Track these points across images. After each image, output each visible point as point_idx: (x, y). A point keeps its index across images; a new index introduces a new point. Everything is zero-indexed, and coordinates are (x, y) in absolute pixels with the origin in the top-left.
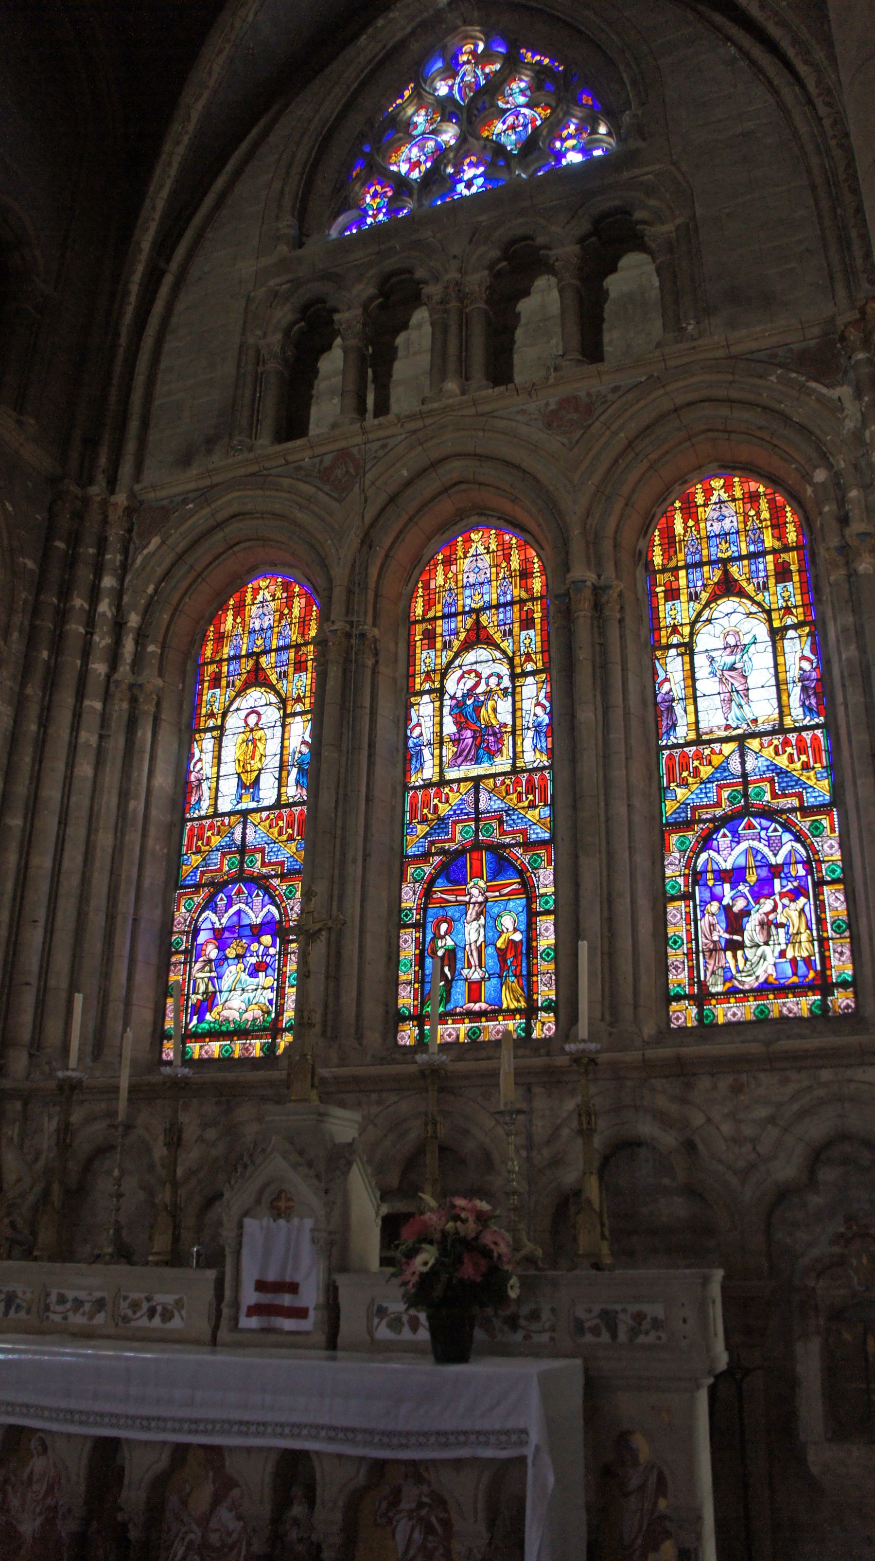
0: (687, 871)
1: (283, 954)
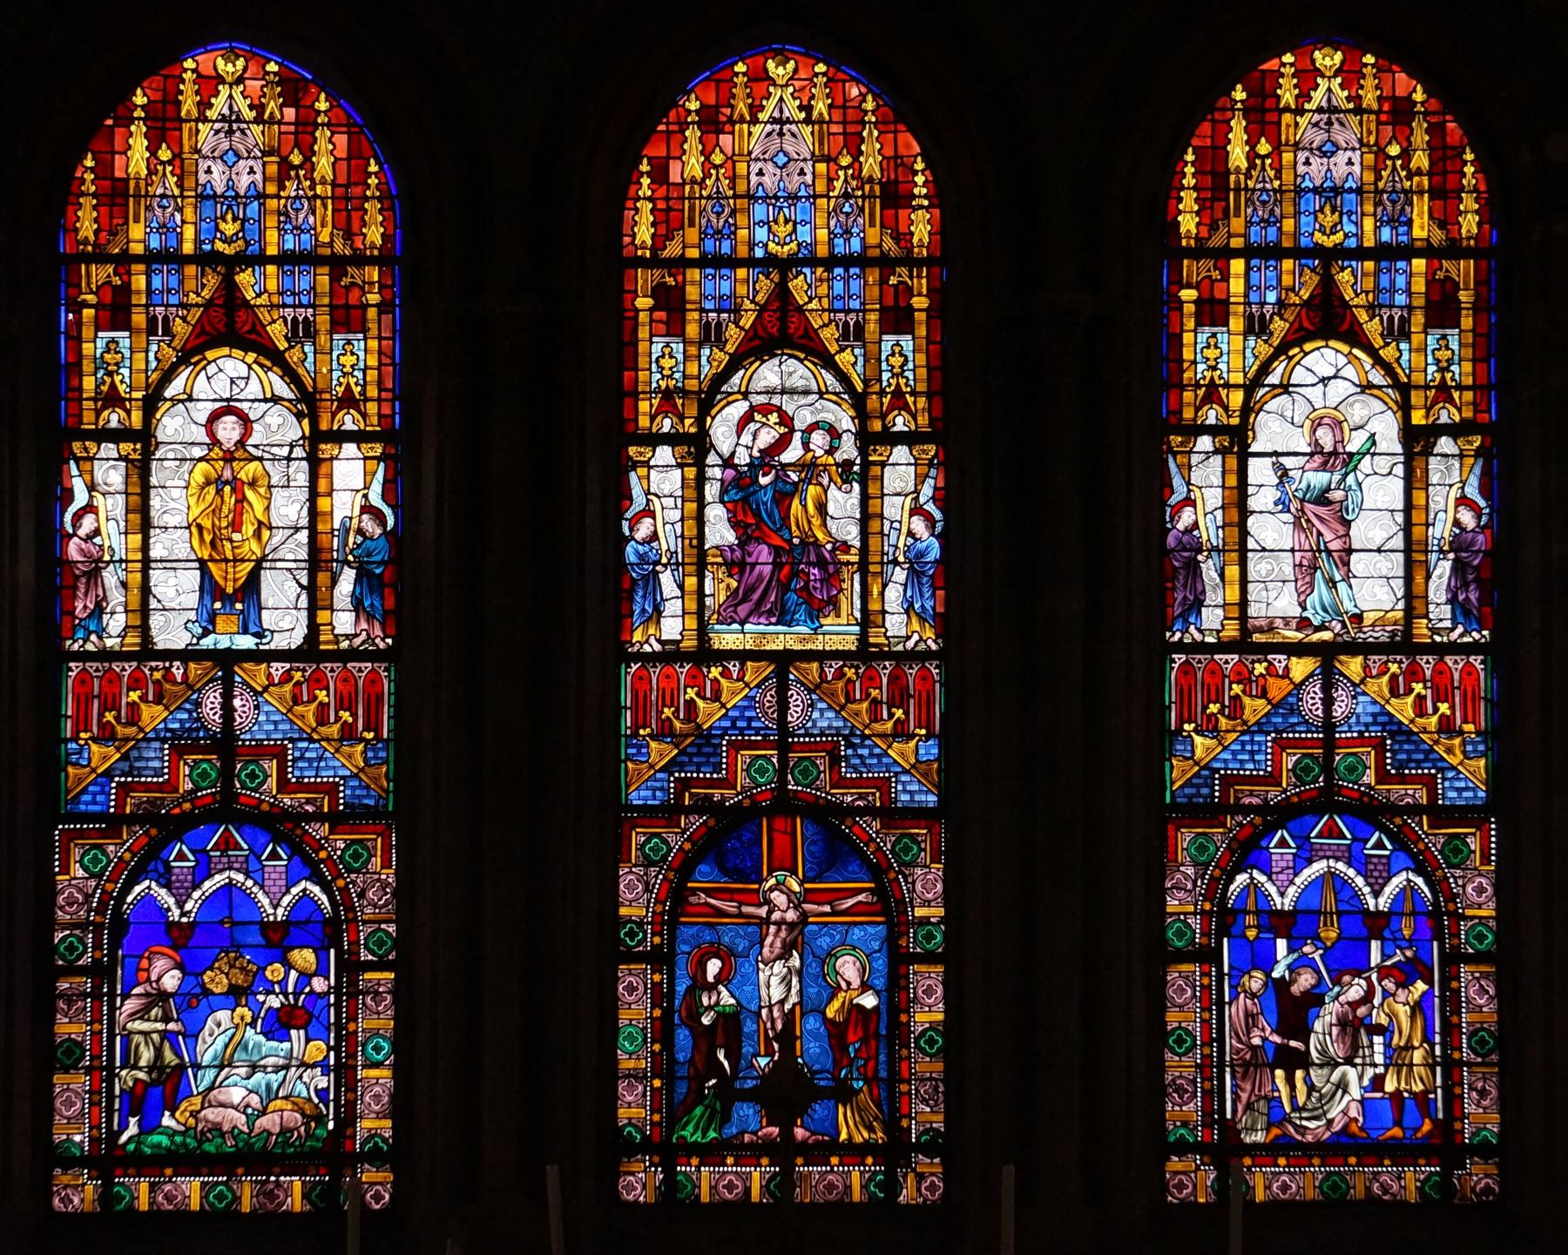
0: (1207, 906)
1: (349, 990)
